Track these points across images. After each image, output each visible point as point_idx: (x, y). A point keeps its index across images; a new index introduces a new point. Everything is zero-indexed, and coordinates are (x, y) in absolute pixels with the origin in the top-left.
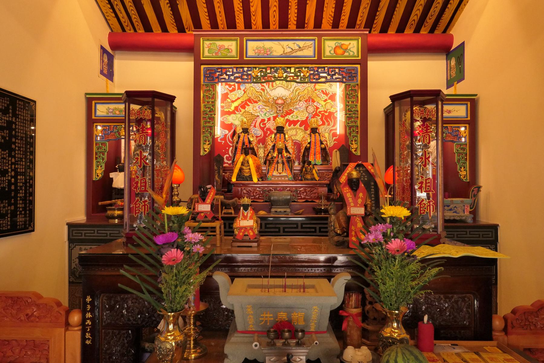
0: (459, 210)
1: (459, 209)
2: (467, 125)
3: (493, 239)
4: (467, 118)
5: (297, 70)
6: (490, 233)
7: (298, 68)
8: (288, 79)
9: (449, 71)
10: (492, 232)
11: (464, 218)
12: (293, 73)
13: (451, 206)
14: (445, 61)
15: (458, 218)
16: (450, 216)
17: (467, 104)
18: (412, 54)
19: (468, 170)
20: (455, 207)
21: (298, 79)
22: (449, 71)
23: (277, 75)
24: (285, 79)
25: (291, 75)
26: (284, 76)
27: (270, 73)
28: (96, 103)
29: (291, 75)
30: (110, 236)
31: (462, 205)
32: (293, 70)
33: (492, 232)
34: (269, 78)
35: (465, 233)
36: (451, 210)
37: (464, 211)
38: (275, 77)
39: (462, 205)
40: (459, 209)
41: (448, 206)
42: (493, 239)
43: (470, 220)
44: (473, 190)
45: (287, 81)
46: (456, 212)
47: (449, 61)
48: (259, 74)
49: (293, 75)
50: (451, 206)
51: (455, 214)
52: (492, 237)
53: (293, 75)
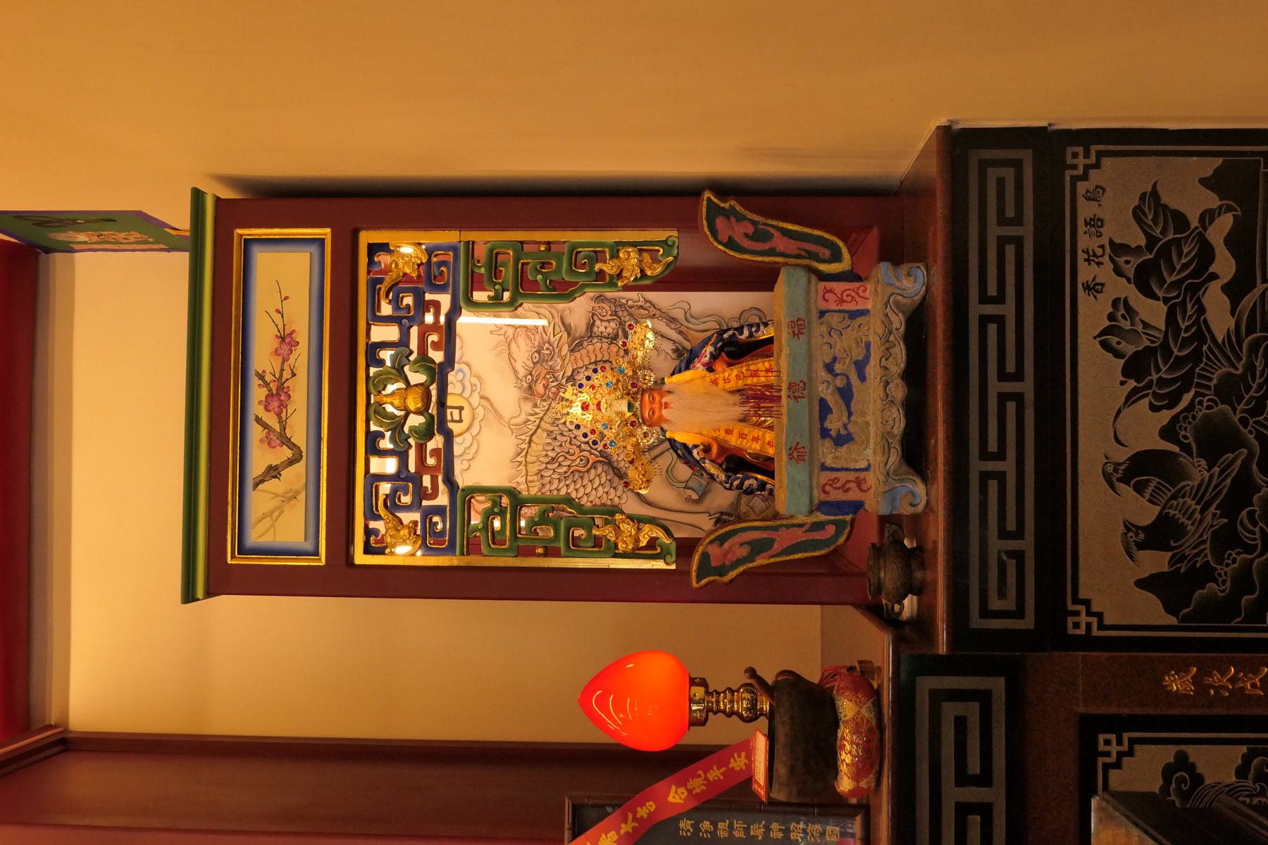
0: (847, 345)
1: (840, 345)
2: (367, 237)
3: (1026, 156)
4: (322, 241)
5: (386, 309)
6: (993, 174)
7: (374, 306)
8: (438, 356)
9: (123, 247)
10: (984, 165)
11: (898, 322)
12: (405, 335)
13: (825, 391)
14: (77, 255)
15: (900, 352)
16: (888, 400)
17: (248, 243)
18: (36, 513)
19: (611, 237)
20: (829, 368)
21: (437, 305)
22: (123, 247)
23: (415, 421)
24: (439, 374)
25: (414, 345)
26: (417, 378)
27: (403, 457)
28: (243, 550)
29: (414, 345)
30: (1019, 376)
31: (819, 330)
32: (388, 333)
33: (984, 165)
34: (431, 461)
35: (1010, 250)
36: (846, 394)
37: (853, 315)
38: (426, 433)
39: (819, 330)
40: (840, 345)
41: (825, 409)
42: (1026, 156)
43: (906, 283)
44: (731, 244)
45: (450, 361)
46: (860, 367)
47: (76, 247)
48: (407, 517)
49: (414, 331)
50: (825, 391)
51: (872, 370)
52: (1017, 165)
53: (414, 331)
